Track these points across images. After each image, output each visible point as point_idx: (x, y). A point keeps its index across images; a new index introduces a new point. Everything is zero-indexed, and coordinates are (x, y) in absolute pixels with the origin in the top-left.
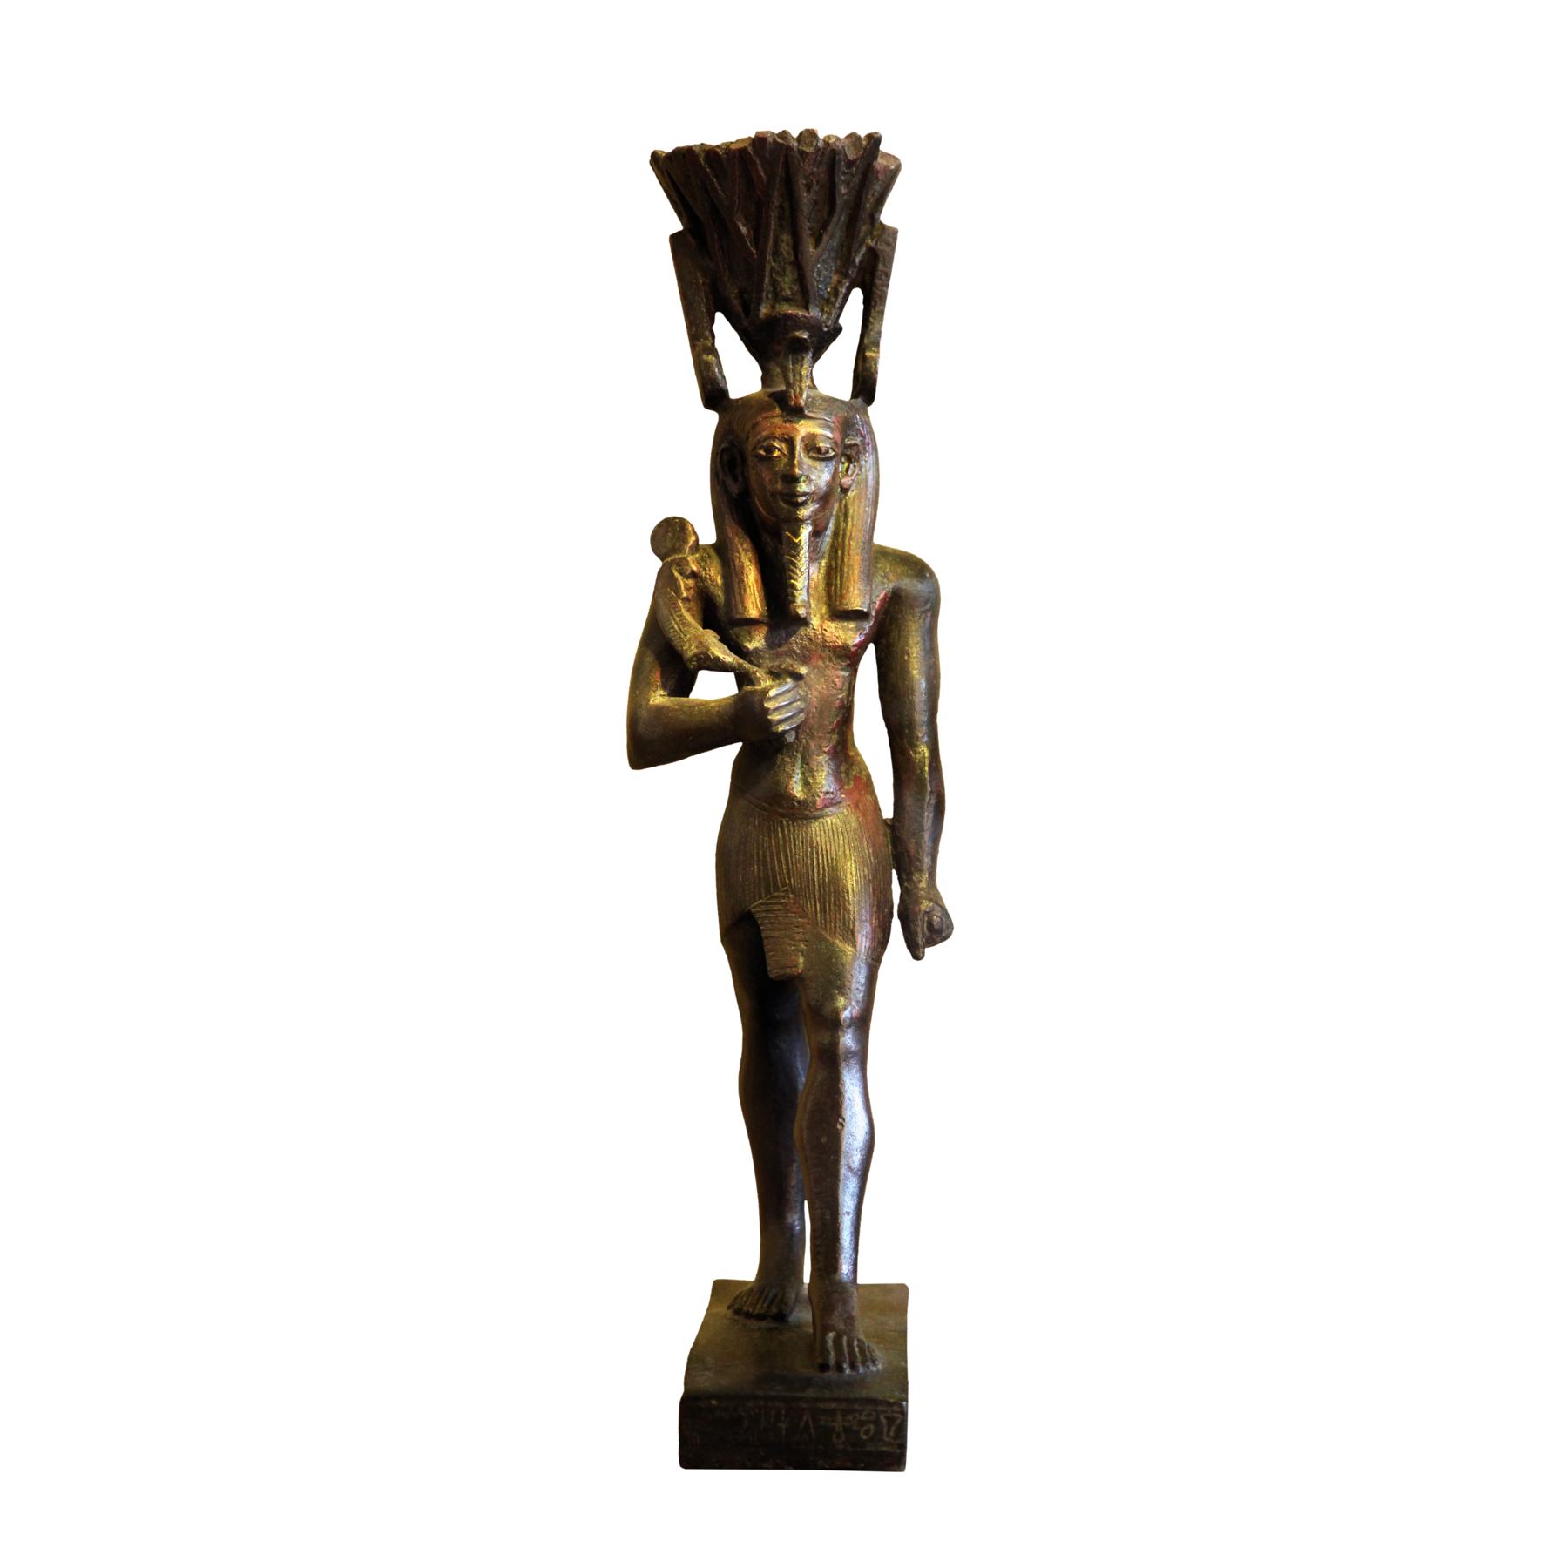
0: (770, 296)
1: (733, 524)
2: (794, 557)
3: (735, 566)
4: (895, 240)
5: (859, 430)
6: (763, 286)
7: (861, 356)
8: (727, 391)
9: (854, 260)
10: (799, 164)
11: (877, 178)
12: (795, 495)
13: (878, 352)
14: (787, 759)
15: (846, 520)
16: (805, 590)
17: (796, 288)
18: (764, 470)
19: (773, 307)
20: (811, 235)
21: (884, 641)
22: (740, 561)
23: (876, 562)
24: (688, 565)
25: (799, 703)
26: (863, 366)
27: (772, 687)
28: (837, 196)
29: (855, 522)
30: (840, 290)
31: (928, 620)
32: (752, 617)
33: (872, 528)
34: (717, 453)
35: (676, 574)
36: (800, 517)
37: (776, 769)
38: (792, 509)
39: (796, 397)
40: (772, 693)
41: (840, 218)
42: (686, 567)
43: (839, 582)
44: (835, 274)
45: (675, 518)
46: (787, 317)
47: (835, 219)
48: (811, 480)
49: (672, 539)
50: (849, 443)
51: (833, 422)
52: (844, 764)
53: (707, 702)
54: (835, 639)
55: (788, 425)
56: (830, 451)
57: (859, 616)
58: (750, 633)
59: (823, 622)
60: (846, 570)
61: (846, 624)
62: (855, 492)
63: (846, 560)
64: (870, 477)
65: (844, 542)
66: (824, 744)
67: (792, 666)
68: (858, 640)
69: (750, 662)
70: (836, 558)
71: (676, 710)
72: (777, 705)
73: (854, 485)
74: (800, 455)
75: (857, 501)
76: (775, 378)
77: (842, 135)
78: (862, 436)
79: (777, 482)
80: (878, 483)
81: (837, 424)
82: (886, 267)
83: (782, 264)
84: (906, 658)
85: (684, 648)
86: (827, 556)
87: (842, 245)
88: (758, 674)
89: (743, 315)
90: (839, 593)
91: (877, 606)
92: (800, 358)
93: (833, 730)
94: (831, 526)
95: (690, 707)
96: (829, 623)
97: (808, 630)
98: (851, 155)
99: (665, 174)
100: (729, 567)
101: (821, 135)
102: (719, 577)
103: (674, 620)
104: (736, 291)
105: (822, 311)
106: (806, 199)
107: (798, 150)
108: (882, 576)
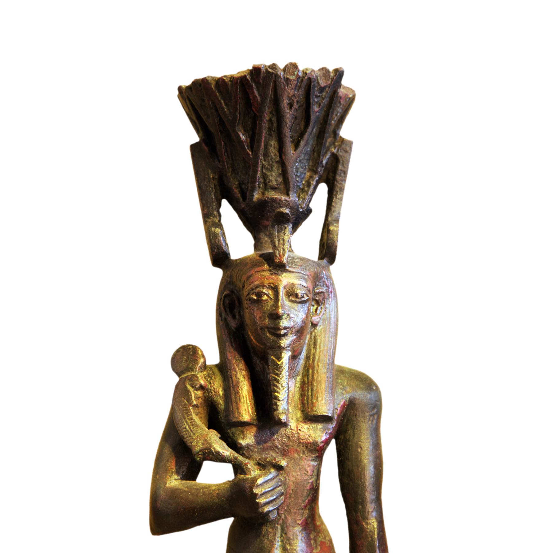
0: (261, 186)
1: (232, 350)
2: (277, 375)
3: (232, 381)
4: (351, 148)
5: (324, 282)
6: (256, 179)
7: (326, 229)
8: (229, 254)
9: (322, 161)
10: (285, 89)
11: (340, 102)
12: (279, 329)
13: (338, 227)
14: (270, 530)
15: (315, 348)
16: (285, 400)
17: (280, 180)
18: (255, 310)
19: (263, 194)
20: (292, 142)
21: (342, 437)
22: (236, 378)
23: (337, 379)
24: (198, 381)
25: (280, 488)
26: (327, 236)
27: (260, 476)
28: (311, 113)
29: (322, 349)
30: (312, 182)
31: (375, 421)
32: (245, 420)
33: (334, 354)
34: (221, 298)
35: (189, 387)
36: (283, 345)
37: (262, 538)
38: (276, 339)
39: (280, 256)
40: (260, 481)
41: (313, 130)
42: (196, 382)
43: (310, 394)
44: (308, 171)
45: (189, 345)
46: (274, 200)
47: (309, 130)
48: (290, 318)
49: (186, 361)
50: (318, 291)
51: (307, 275)
52: (313, 532)
53: (210, 486)
54: (307, 437)
55: (273, 276)
56: (305, 296)
57: (325, 419)
58: (243, 432)
59: (299, 424)
60: (315, 385)
61: (315, 425)
62: (321, 327)
63: (315, 377)
64: (333, 316)
65: (313, 363)
66: (299, 518)
67: (275, 460)
68: (324, 438)
69: (243, 455)
70: (308, 375)
71: (186, 492)
72: (263, 491)
73: (321, 322)
74: (282, 299)
75: (323, 334)
76: (264, 245)
77: (316, 69)
78: (327, 286)
79: (265, 319)
80: (337, 320)
81: (310, 276)
82: (345, 168)
83: (271, 163)
84: (359, 450)
85: (193, 444)
86: (301, 373)
87: (314, 151)
88: (249, 465)
89: (241, 200)
90: (310, 402)
91: (338, 411)
92: (284, 228)
93: (305, 507)
94: (304, 352)
95: (197, 489)
96: (303, 425)
97: (287, 430)
98: (322, 83)
99: (187, 101)
100: (228, 382)
101: (301, 68)
102: (221, 389)
103: (186, 422)
104: (237, 183)
105: (299, 197)
106: (288, 115)
107: (284, 77)
108: (341, 389)
